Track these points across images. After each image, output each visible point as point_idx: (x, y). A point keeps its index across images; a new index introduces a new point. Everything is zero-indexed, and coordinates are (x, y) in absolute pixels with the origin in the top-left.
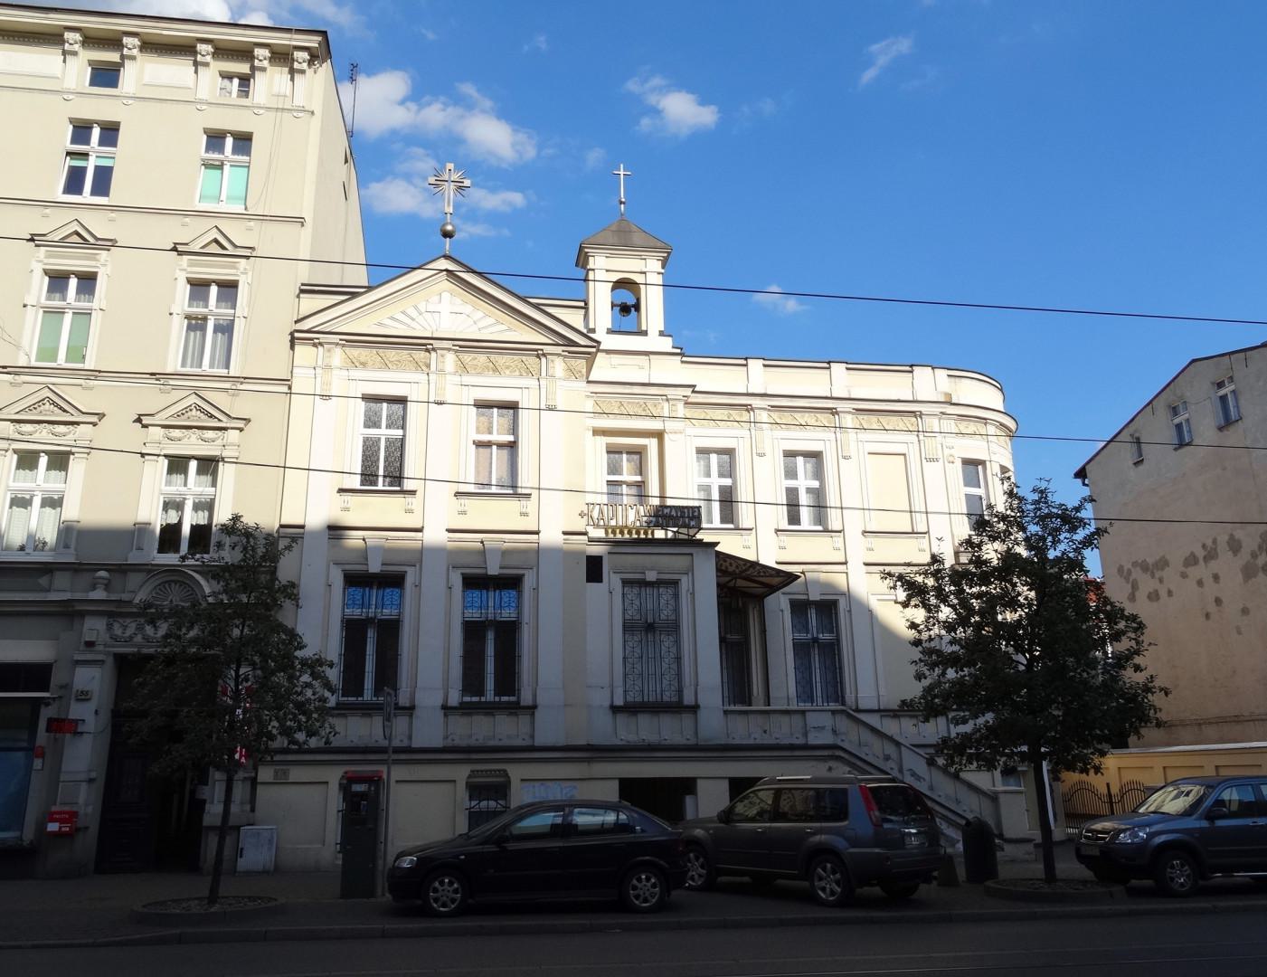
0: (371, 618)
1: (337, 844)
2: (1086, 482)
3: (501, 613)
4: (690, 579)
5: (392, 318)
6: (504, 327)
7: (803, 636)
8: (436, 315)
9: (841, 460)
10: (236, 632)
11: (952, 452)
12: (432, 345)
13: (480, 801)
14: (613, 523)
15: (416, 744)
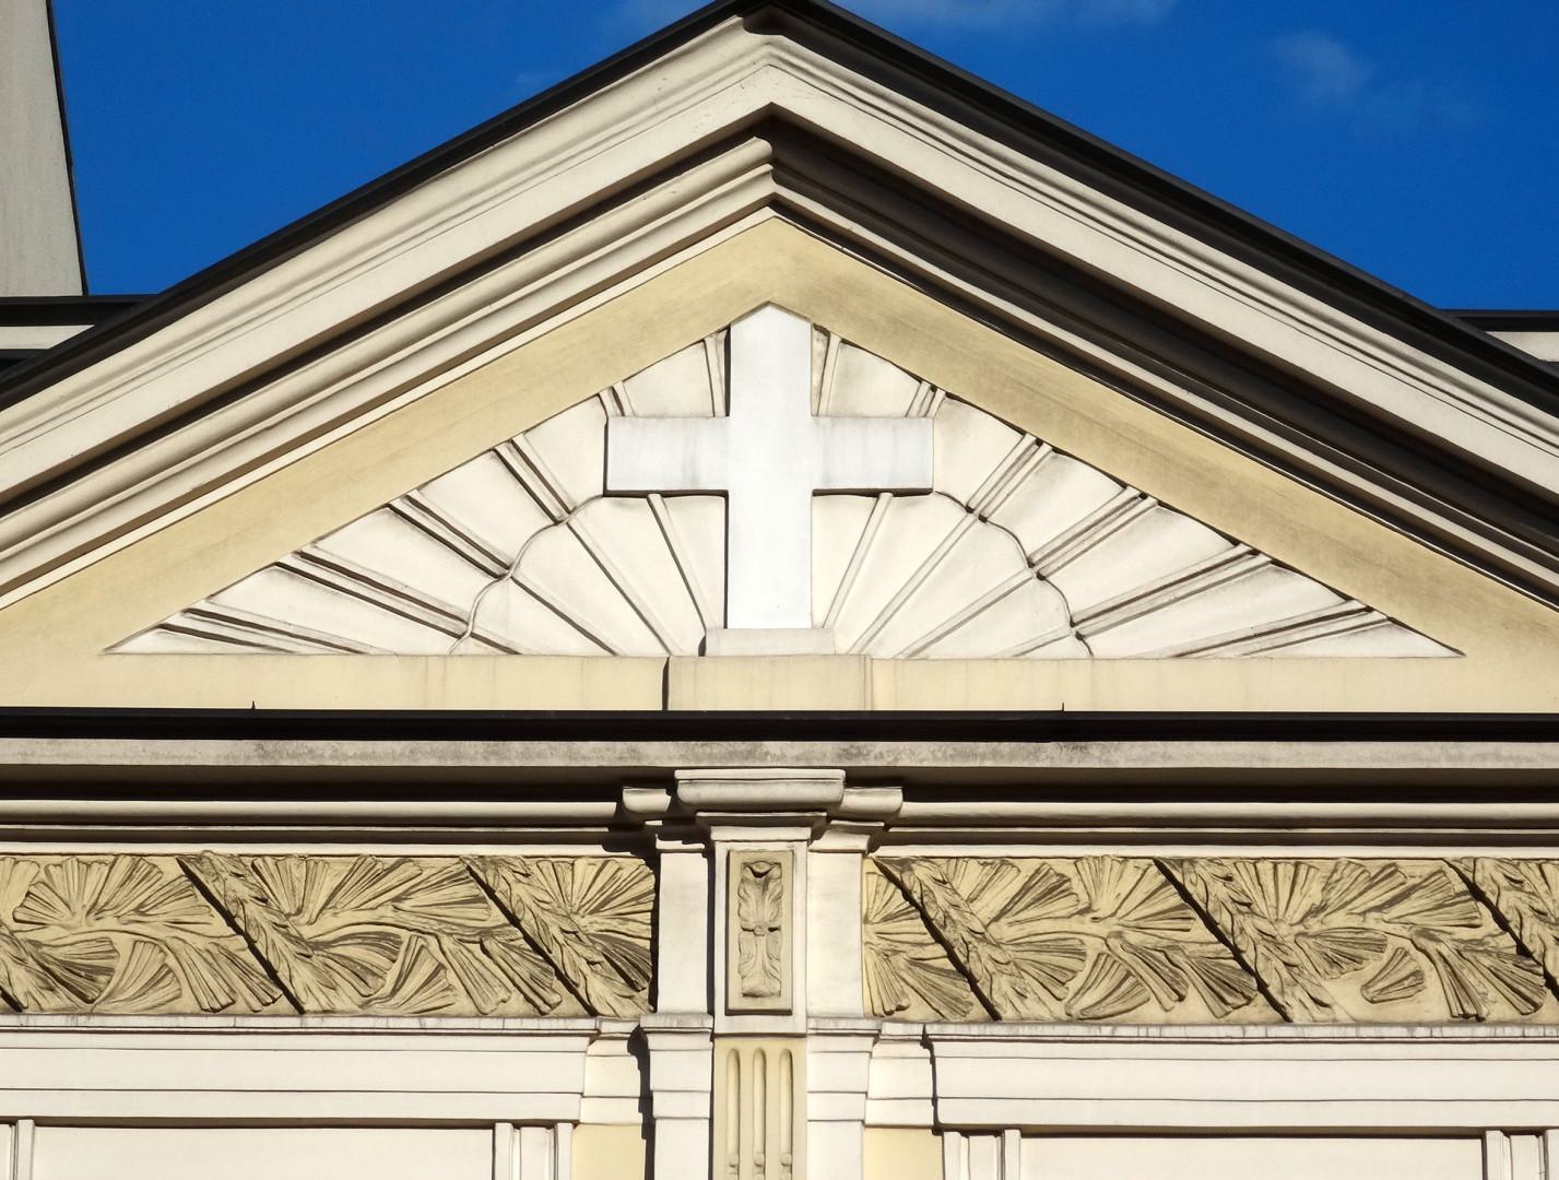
5: (312, 568)
6: (1297, 597)
8: (696, 523)
12: (663, 779)
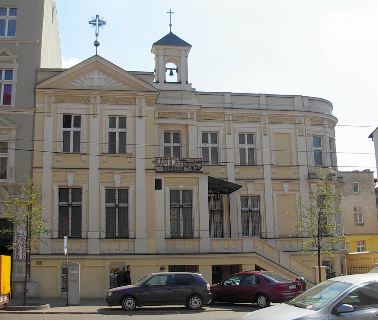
1: (61, 289)
2: (373, 140)
4: (197, 187)
7: (245, 209)
9: (263, 136)
11: (310, 132)
14: (166, 165)
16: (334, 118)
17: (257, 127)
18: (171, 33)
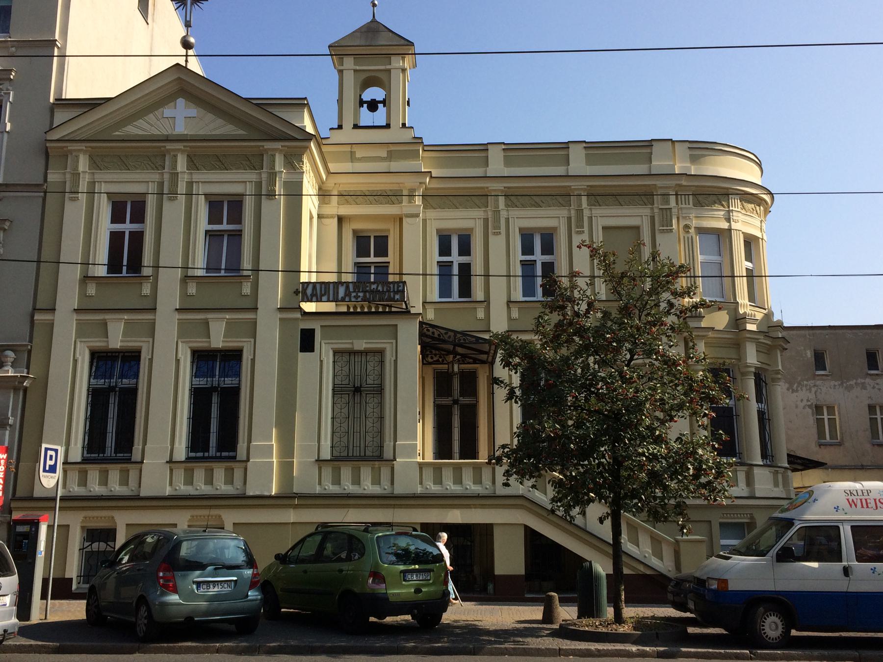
0: (215, 387)
3: (224, 381)
10: (624, 411)
13: (92, 543)
15: (142, 494)
16: (152, 80)
17: (561, 216)
18: (374, 21)
